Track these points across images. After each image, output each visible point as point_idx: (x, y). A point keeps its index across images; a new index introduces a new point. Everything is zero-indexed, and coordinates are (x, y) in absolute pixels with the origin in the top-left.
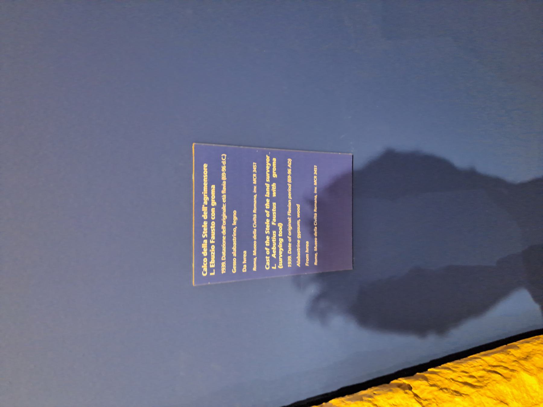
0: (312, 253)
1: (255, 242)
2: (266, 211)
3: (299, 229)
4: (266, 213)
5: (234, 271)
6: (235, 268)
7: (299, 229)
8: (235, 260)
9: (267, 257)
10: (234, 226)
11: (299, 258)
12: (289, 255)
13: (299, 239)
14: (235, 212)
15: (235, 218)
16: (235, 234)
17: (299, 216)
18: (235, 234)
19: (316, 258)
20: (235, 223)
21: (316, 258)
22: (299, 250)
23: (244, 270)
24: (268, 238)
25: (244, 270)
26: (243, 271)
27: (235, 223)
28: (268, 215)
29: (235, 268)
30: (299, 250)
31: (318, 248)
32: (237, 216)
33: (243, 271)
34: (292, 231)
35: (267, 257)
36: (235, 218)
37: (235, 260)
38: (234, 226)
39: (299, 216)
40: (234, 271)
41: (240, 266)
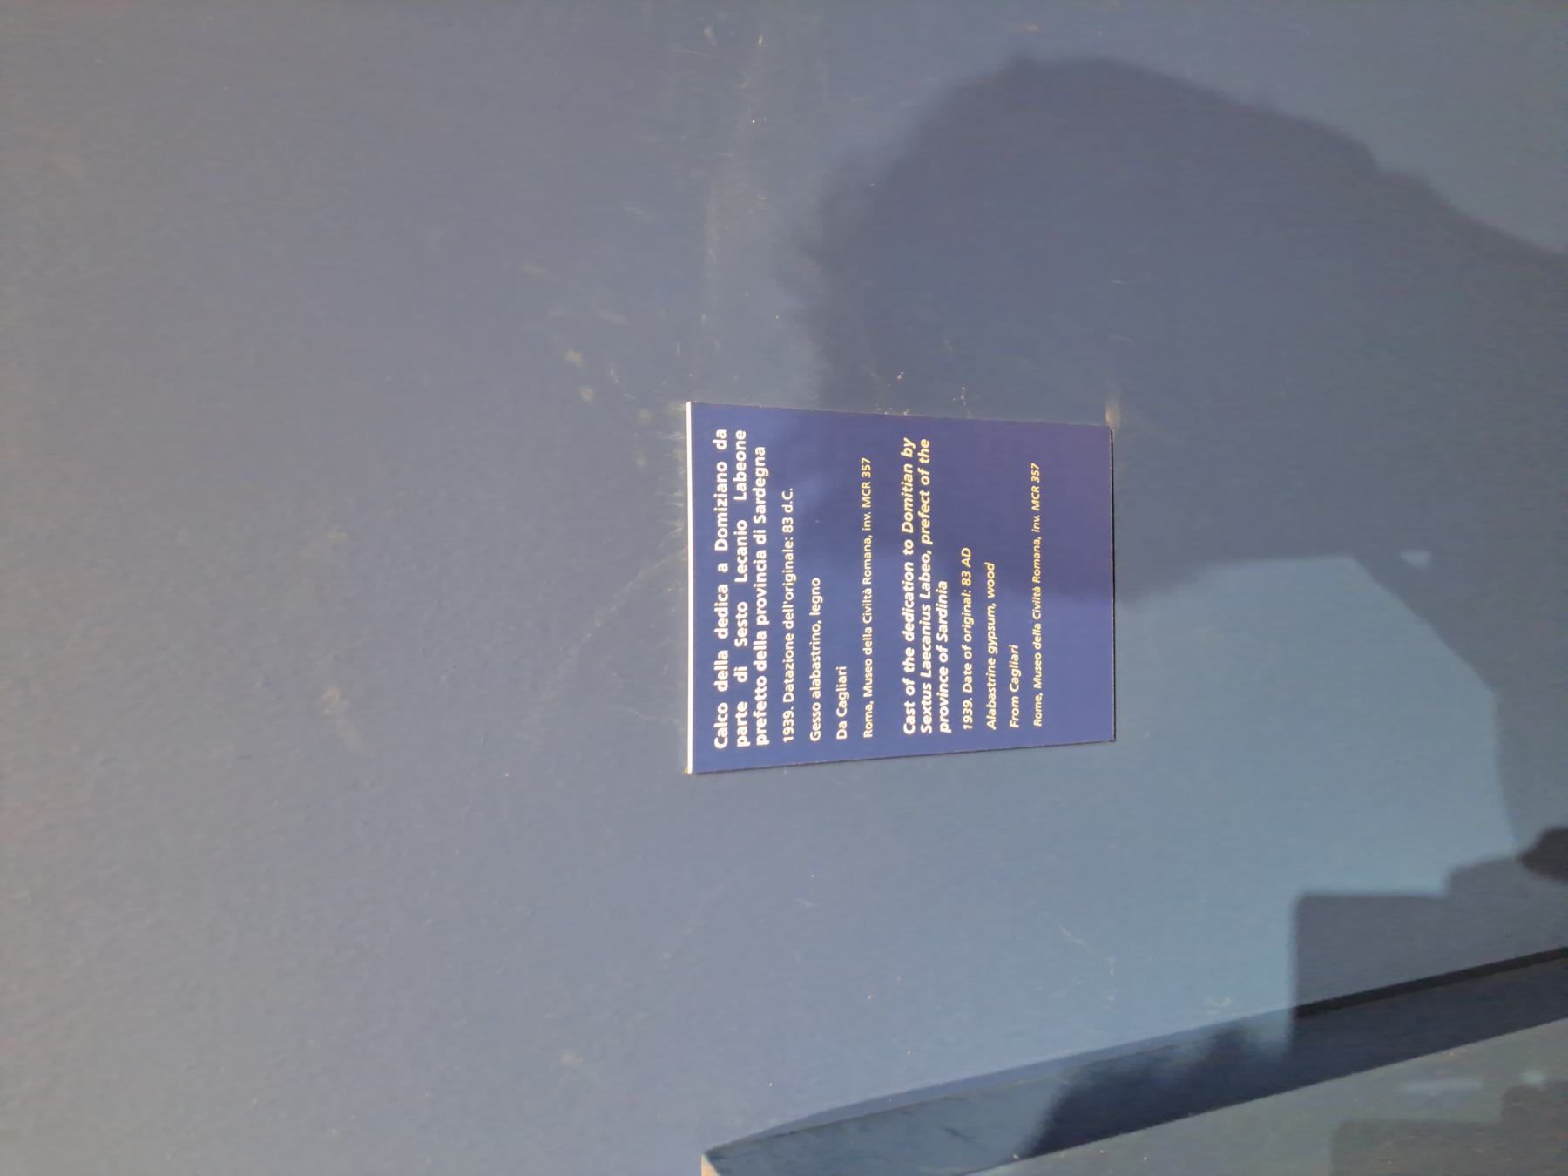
0: (1027, 693)
1: (868, 663)
2: (906, 681)
3: (991, 628)
4: (905, 686)
5: (816, 735)
6: (816, 727)
7: (991, 628)
8: (816, 709)
9: (907, 704)
10: (815, 619)
11: (992, 706)
12: (967, 696)
13: (993, 656)
14: (816, 583)
15: (817, 599)
16: (816, 640)
17: (991, 594)
18: (816, 640)
19: (1038, 707)
20: (816, 610)
21: (1038, 707)
22: (991, 683)
23: (842, 733)
24: (910, 652)
25: (842, 733)
26: (717, 548)
27: (816, 610)
28: (910, 691)
29: (816, 727)
30: (991, 683)
31: (1043, 679)
32: (822, 592)
33: (717, 548)
34: (973, 629)
35: (907, 704)
36: (817, 599)
37: (816, 709)
38: (815, 619)
39: (991, 594)
40: (816, 735)
41: (830, 724)
